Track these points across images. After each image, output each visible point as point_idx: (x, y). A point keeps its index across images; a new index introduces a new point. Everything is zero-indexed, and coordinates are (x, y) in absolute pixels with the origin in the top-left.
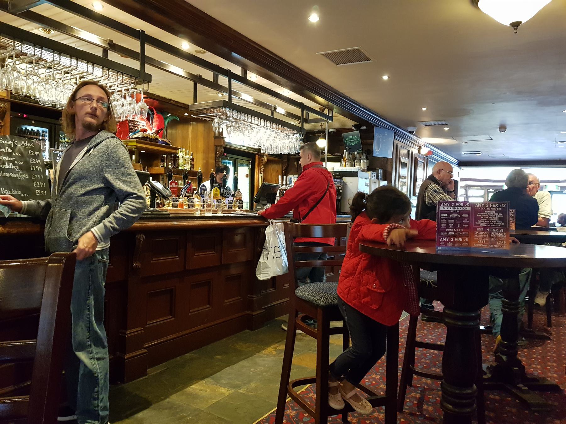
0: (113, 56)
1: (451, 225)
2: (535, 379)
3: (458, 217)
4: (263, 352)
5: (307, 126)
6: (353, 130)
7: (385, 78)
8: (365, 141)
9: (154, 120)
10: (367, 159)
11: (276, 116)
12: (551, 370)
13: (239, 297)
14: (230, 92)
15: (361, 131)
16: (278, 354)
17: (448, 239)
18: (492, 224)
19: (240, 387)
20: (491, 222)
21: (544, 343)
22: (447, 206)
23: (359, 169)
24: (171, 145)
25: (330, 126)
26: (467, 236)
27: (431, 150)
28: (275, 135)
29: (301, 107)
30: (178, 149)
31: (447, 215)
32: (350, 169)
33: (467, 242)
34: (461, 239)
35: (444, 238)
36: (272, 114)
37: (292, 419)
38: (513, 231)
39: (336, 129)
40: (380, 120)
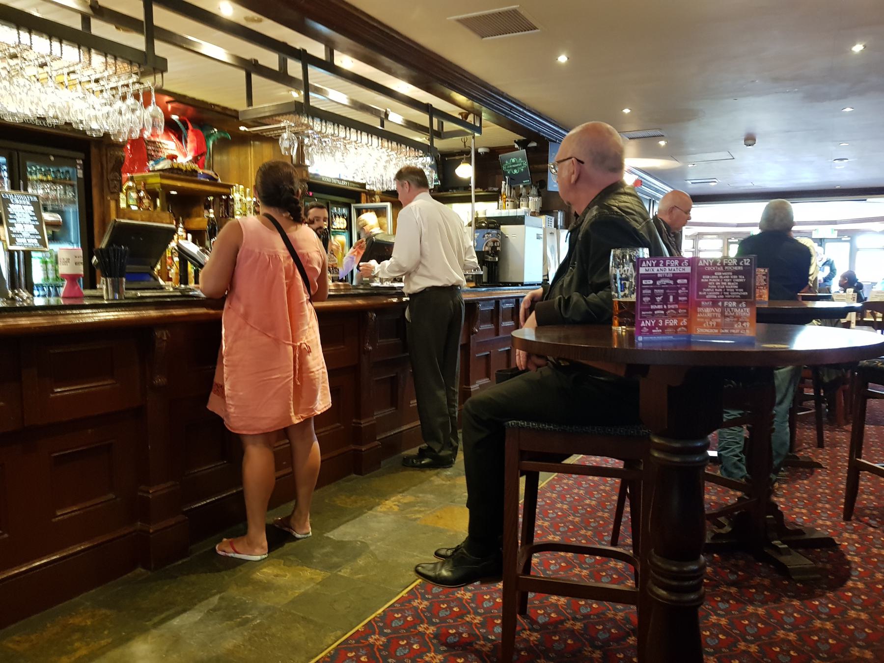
0: (101, 29)
1: (659, 299)
2: (800, 532)
3: (671, 284)
4: (379, 508)
5: (439, 144)
6: (517, 149)
7: (563, 59)
8: (536, 166)
9: (188, 140)
10: (539, 195)
11: (388, 127)
12: (822, 514)
13: (338, 424)
14: (307, 87)
15: (529, 150)
16: (402, 510)
17: (653, 322)
18: (728, 293)
19: (340, 566)
20: (726, 291)
21: (812, 473)
22: (652, 266)
23: (526, 213)
24: (220, 181)
25: (480, 142)
26: (686, 315)
27: (641, 179)
28: (388, 158)
29: (428, 112)
30: (232, 186)
31: (651, 282)
32: (512, 212)
33: (684, 326)
34: (675, 322)
35: (648, 321)
36: (382, 125)
37: (422, 615)
38: (764, 302)
39: (489, 148)
40: (558, 131)
